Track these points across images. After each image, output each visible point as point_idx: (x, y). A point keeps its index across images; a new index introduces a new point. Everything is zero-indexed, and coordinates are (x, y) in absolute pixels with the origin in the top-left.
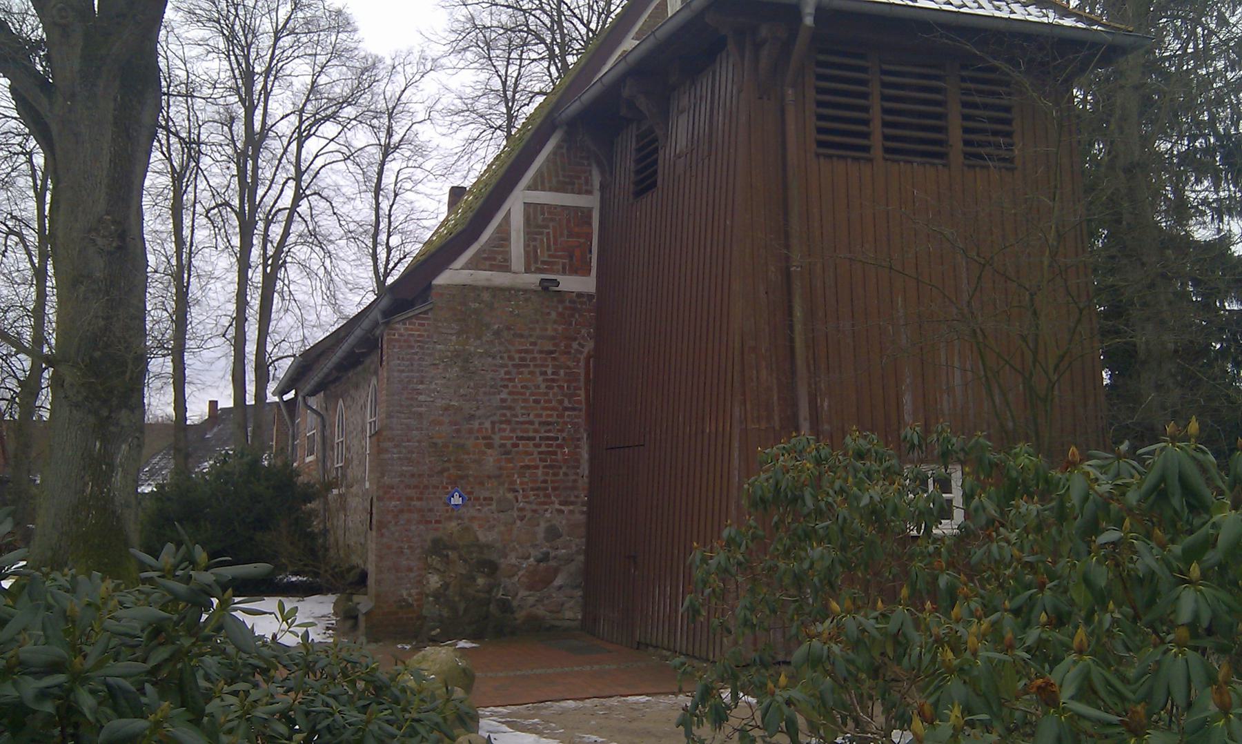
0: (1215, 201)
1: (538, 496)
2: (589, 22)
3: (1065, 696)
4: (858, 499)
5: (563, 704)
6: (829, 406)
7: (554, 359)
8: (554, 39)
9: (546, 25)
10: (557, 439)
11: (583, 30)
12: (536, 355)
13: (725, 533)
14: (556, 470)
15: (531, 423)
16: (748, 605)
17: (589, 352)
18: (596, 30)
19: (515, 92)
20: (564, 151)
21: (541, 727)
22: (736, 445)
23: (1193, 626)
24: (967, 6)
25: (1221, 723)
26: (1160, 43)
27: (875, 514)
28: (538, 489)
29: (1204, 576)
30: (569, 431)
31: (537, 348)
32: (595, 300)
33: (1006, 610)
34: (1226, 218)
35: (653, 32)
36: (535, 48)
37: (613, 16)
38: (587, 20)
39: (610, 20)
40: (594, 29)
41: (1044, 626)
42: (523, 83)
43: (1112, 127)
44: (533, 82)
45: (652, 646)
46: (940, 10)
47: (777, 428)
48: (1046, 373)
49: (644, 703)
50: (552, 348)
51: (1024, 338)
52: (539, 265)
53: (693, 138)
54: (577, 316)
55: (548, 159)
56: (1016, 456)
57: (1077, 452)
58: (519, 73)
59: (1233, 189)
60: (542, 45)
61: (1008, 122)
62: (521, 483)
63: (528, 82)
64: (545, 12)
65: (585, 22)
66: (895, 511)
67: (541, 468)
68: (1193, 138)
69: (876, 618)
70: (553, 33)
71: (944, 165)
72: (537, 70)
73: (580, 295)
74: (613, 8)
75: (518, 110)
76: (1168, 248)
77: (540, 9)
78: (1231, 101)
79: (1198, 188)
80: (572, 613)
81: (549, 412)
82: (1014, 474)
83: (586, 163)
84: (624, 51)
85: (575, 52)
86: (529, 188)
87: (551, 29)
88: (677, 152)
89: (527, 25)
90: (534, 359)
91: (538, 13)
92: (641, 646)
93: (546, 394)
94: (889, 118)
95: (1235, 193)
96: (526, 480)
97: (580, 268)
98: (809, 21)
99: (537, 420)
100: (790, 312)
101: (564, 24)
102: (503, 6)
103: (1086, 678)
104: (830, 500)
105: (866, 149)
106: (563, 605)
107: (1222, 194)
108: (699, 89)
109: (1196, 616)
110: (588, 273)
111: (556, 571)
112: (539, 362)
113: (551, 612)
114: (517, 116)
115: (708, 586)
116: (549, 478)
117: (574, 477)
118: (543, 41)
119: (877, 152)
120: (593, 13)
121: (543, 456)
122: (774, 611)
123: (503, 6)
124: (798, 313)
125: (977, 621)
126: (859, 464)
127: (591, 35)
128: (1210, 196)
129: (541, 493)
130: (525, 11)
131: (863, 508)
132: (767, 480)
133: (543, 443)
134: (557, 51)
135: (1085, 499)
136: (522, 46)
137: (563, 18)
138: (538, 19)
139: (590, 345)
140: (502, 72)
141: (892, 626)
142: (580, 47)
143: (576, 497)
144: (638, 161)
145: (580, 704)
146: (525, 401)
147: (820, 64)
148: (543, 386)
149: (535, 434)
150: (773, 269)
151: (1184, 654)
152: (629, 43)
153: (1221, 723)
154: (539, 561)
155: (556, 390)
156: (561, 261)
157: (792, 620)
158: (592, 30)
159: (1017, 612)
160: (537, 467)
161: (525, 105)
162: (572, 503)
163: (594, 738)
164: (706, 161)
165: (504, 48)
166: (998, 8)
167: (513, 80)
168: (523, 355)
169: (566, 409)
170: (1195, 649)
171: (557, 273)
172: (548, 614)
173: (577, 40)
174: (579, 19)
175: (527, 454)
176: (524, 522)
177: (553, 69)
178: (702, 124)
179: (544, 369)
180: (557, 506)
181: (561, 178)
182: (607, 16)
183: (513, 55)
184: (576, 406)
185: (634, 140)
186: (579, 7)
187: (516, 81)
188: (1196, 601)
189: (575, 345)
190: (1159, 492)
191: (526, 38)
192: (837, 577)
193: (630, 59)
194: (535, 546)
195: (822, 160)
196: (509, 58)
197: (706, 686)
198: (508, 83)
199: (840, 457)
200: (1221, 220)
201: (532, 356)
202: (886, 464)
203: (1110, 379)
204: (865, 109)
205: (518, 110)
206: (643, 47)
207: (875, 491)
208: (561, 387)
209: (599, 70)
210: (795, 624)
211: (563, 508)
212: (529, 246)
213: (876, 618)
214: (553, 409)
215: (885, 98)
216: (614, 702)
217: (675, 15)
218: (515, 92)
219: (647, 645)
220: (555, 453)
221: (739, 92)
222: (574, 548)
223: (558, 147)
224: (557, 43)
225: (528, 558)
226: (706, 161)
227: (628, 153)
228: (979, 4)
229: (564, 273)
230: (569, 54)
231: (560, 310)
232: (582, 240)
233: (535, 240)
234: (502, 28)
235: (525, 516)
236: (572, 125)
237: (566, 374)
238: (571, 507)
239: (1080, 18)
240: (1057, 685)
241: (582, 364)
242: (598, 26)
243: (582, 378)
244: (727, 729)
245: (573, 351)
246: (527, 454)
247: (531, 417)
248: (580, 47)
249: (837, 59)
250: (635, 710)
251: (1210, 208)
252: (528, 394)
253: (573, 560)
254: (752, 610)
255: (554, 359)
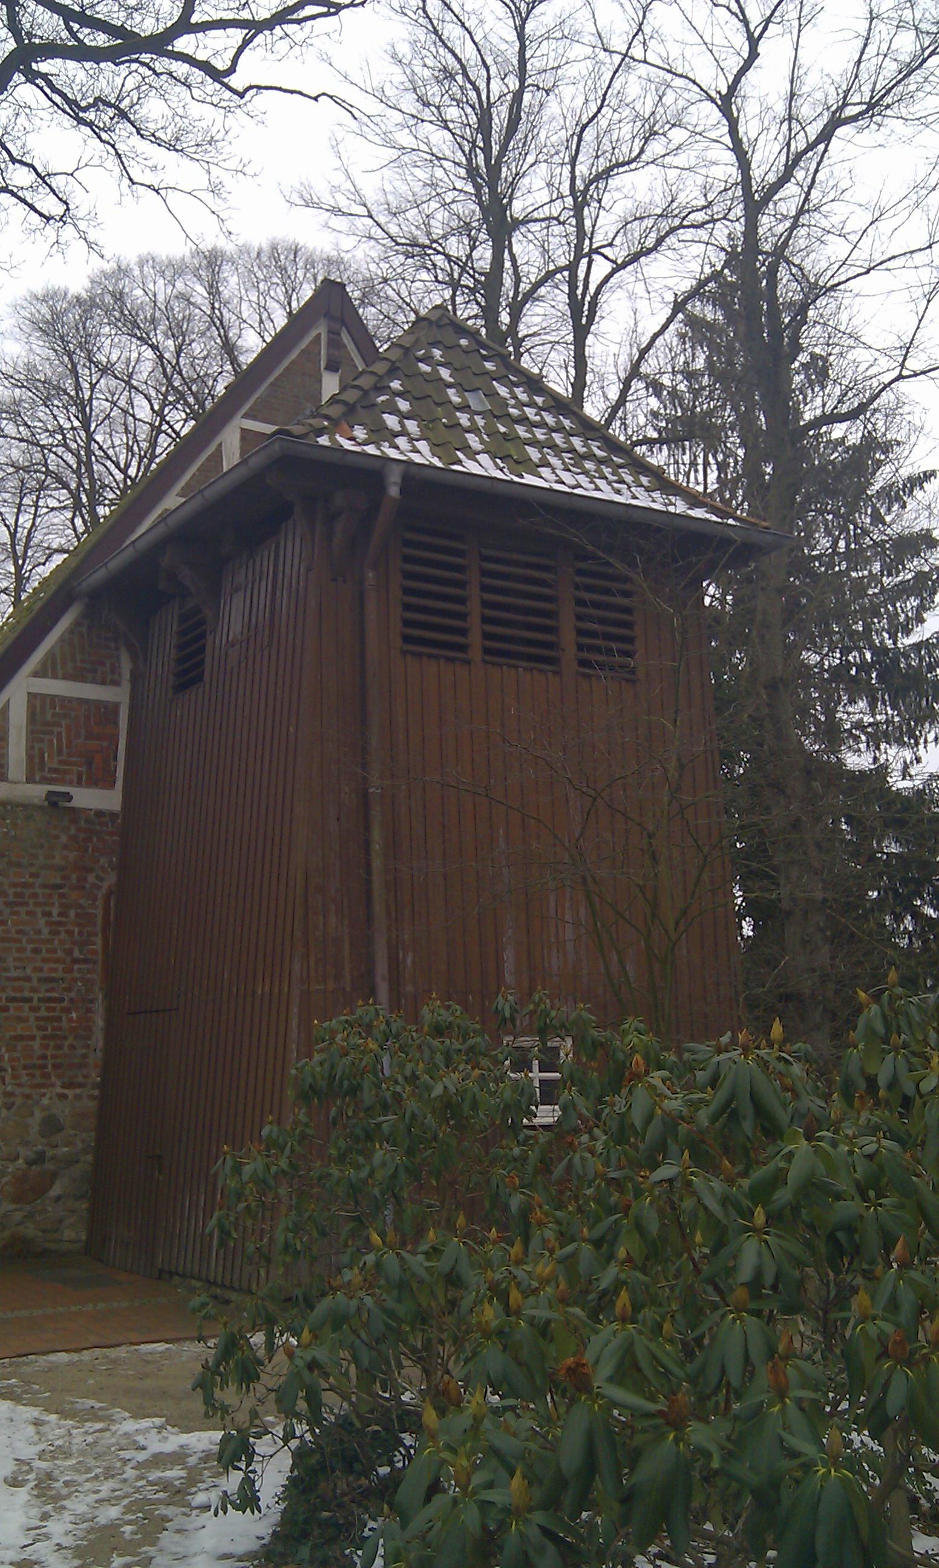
0: (870, 725)
1: (33, 1076)
2: (128, 465)
3: (600, 1378)
4: (429, 1089)
5: (52, 1357)
6: (414, 962)
7: (62, 896)
8: (80, 484)
9: (70, 467)
10: (62, 1000)
11: (120, 476)
12: (38, 891)
13: (265, 1132)
14: (59, 1042)
15: (28, 979)
16: (291, 1226)
17: (109, 887)
18: (137, 476)
19: (27, 547)
20: (84, 629)
21: (19, 1391)
22: (295, 1010)
23: (755, 1285)
24: (581, 487)
25: (776, 1409)
26: (809, 540)
27: (449, 1107)
28: (34, 1066)
29: (770, 1219)
30: (79, 990)
31: (40, 881)
32: (119, 821)
33: (584, 1240)
34: (883, 746)
35: (201, 491)
36: (55, 493)
37: (157, 460)
38: (126, 464)
39: (154, 466)
40: (133, 475)
41: (622, 1263)
42: (38, 537)
43: (754, 634)
44: (51, 536)
45: (177, 1274)
46: (551, 490)
47: (348, 989)
48: (666, 932)
49: (161, 1352)
50: (59, 881)
51: (642, 889)
52: (46, 774)
53: (250, 620)
54: (95, 840)
55: (62, 639)
56: (625, 1033)
57: (641, 1061)
58: (33, 524)
59: (890, 712)
60: (65, 491)
61: (628, 625)
62: (11, 1060)
63: (46, 534)
64: (70, 450)
65: (122, 466)
66: (475, 1105)
67: (38, 1039)
68: (846, 651)
69: (426, 1253)
70: (79, 477)
71: (555, 673)
72: (56, 521)
73: (100, 813)
74: (158, 450)
75: (31, 571)
76: (815, 780)
77: (62, 446)
78: (887, 610)
79: (851, 709)
80: (73, 1234)
81: (53, 965)
82: (621, 1056)
83: (112, 645)
84: (166, 510)
85: (107, 502)
86: (36, 674)
87: (77, 472)
88: (230, 639)
89: (46, 465)
90: (34, 895)
91: (60, 450)
92: (164, 1275)
93: (48, 941)
94: (489, 613)
95: (893, 716)
96: (16, 1054)
97: (102, 779)
98: (394, 491)
99: (35, 976)
100: (366, 846)
101: (95, 468)
102: (15, 438)
103: (628, 1350)
104: (399, 1089)
105: (462, 648)
106: (61, 1221)
107: (878, 717)
108: (258, 564)
109: (758, 1274)
110: (111, 785)
111: (53, 1176)
112: (41, 899)
113: (44, 1231)
114: (29, 577)
115: (243, 1199)
116: (49, 1053)
117: (84, 1051)
118: (66, 486)
119: (476, 654)
120: (133, 456)
121: (42, 1023)
122: (323, 1234)
123: (15, 438)
124: (377, 847)
125: (548, 1254)
126: (436, 1043)
127: (129, 483)
128: (865, 719)
129: (38, 1073)
130: (43, 447)
131: (435, 1099)
132: (321, 1064)
133: (43, 1006)
134: (84, 499)
135: (649, 1119)
136: (39, 490)
137: (93, 458)
138: (61, 458)
139: (111, 879)
140: (11, 521)
141: (443, 1264)
142: (114, 496)
143: (85, 1077)
144: (180, 647)
145: (75, 1357)
146: (21, 950)
147: (408, 543)
148: (46, 931)
149: (32, 994)
150: (347, 790)
151: (741, 1318)
152: (172, 501)
153: (776, 1409)
154: (30, 1163)
155: (63, 936)
156: (75, 769)
157: (346, 1245)
158: (130, 477)
159: (597, 1243)
160: (33, 1038)
161: (39, 564)
162: (80, 1085)
163: (91, 1402)
164: (266, 652)
165: (14, 490)
166: (618, 492)
167: (26, 531)
168: (19, 890)
169: (76, 961)
170: (751, 1313)
171: (70, 783)
172: (40, 1234)
173: (111, 488)
174: (113, 462)
175: (20, 1019)
176: (13, 1110)
177: (78, 521)
178: (261, 607)
179: (47, 909)
180: (59, 1090)
181: (79, 664)
182: (151, 461)
183: (26, 501)
184: (89, 957)
185: (176, 619)
186: (114, 447)
187: (29, 532)
188: (760, 1255)
189: (91, 878)
190: (729, 1112)
191: (44, 481)
192: (401, 1189)
193: (172, 521)
194: (25, 1143)
195: (409, 657)
196: (20, 505)
197: (233, 1335)
198: (18, 535)
199: (414, 1034)
200: (878, 748)
201: (32, 891)
202: (471, 1042)
203: (753, 930)
204: (462, 601)
205: (31, 571)
206: (188, 508)
207: (451, 1081)
208: (70, 933)
209: (132, 530)
210: (349, 1250)
211: (66, 1091)
212: (32, 748)
213: (426, 1253)
214: (57, 961)
215: (484, 588)
216: (121, 1352)
217: (231, 470)
218: (27, 547)
219: (171, 1273)
220: (58, 1019)
221: (309, 570)
222: (80, 1145)
223: (77, 623)
224: (85, 490)
225: (17, 1158)
226: (266, 652)
227: (169, 636)
228: (596, 485)
229: (79, 783)
230: (99, 504)
231: (73, 831)
232: (105, 744)
233: (41, 741)
234: (12, 466)
235: (14, 1104)
236: (96, 598)
237: (77, 915)
238: (78, 1091)
239: (714, 510)
240: (590, 1365)
241: (100, 903)
242: (138, 471)
243: (99, 921)
244: (259, 1389)
245: (88, 886)
246: (20, 1019)
247: (29, 971)
248: (114, 496)
249: (427, 539)
250: (147, 1362)
251: (866, 733)
252: (24, 941)
253: (77, 1162)
254: (297, 1229)
255: (62, 896)
